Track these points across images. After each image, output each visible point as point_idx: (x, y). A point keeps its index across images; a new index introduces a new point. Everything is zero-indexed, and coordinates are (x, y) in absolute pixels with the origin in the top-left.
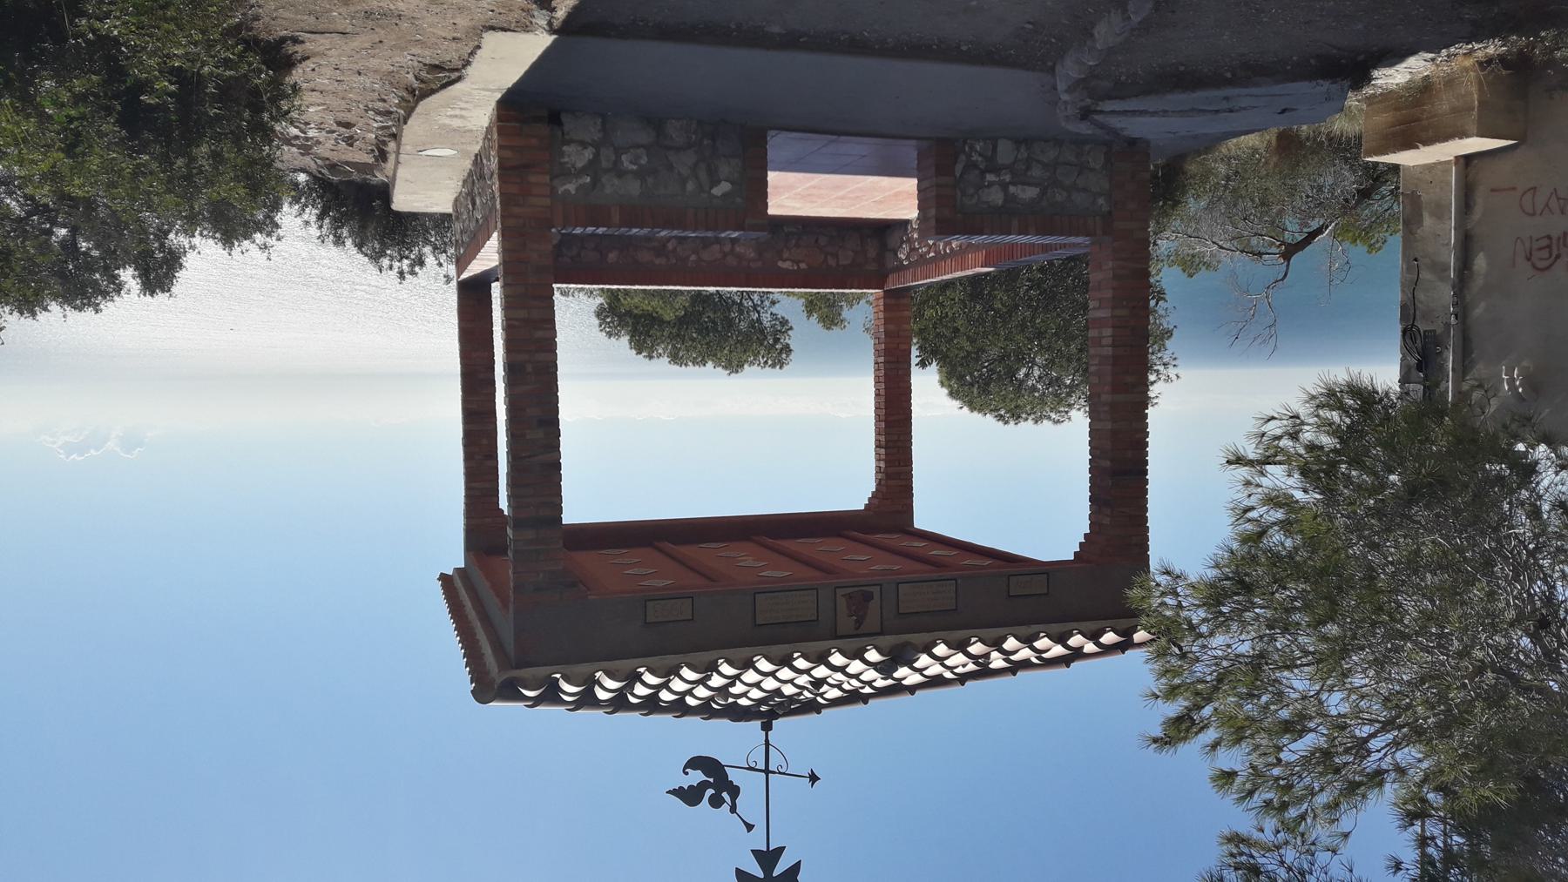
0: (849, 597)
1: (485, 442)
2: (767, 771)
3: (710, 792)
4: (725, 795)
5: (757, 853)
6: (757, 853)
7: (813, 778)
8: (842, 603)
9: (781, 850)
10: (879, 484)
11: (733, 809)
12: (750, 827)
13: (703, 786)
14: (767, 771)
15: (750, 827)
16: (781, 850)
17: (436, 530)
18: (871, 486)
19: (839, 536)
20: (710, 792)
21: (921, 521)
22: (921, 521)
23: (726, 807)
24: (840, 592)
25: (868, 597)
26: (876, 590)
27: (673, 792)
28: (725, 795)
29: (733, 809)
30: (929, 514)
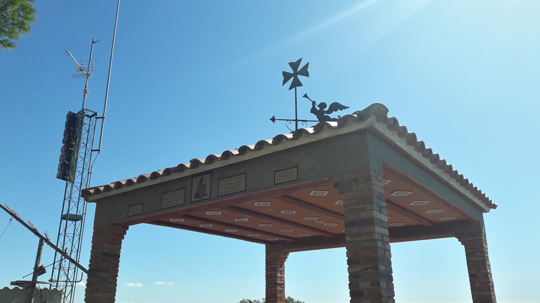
0: (204, 195)
1: (478, 284)
2: (297, 120)
3: (326, 109)
4: (318, 108)
5: (300, 85)
6: (300, 85)
7: (273, 119)
8: (208, 192)
9: (291, 88)
10: (282, 264)
11: (314, 103)
12: (305, 96)
13: (330, 111)
14: (297, 120)
15: (305, 96)
16: (291, 88)
17: (494, 226)
18: (286, 264)
19: (295, 239)
20: (326, 109)
21: (261, 248)
22: (261, 248)
23: (318, 103)
24: (208, 197)
25: (197, 196)
26: (193, 199)
27: (348, 108)
28: (318, 108)
29: (314, 103)
30: (259, 250)
